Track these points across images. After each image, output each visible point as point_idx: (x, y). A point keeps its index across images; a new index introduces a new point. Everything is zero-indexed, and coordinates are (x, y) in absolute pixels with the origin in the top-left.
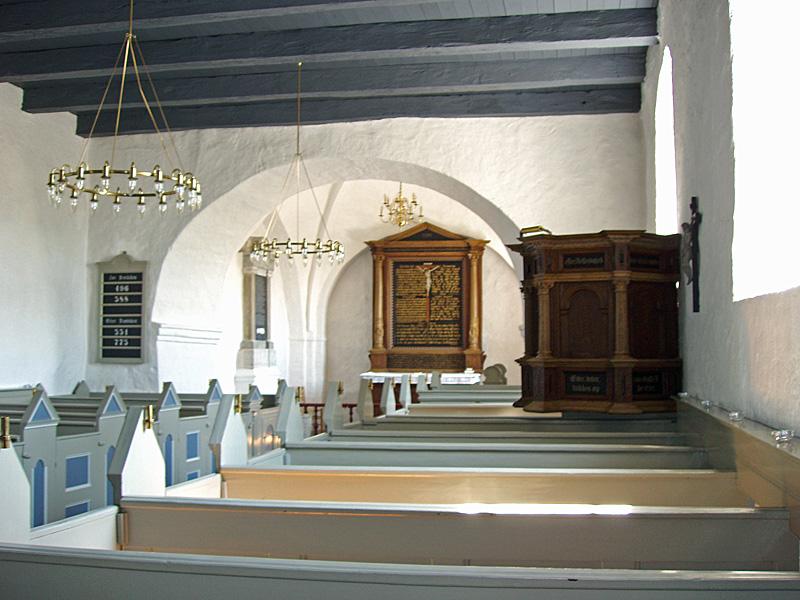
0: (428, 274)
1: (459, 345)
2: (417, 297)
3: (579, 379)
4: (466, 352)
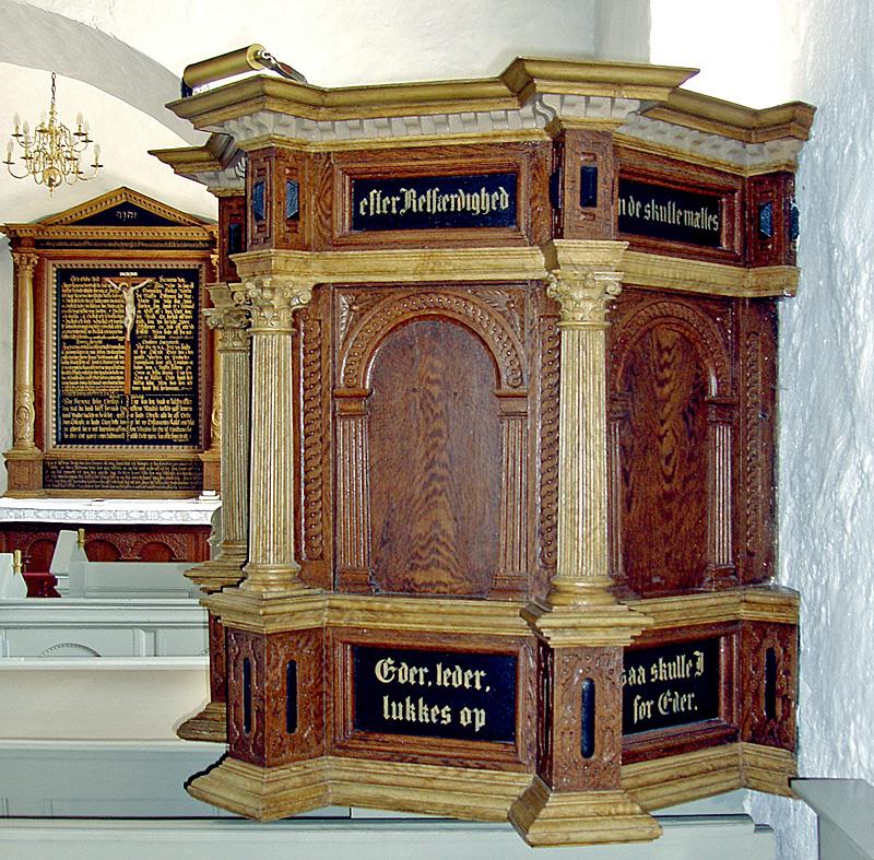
0: (129, 296)
1: (193, 440)
2: (105, 342)
3: (408, 674)
4: (205, 457)
